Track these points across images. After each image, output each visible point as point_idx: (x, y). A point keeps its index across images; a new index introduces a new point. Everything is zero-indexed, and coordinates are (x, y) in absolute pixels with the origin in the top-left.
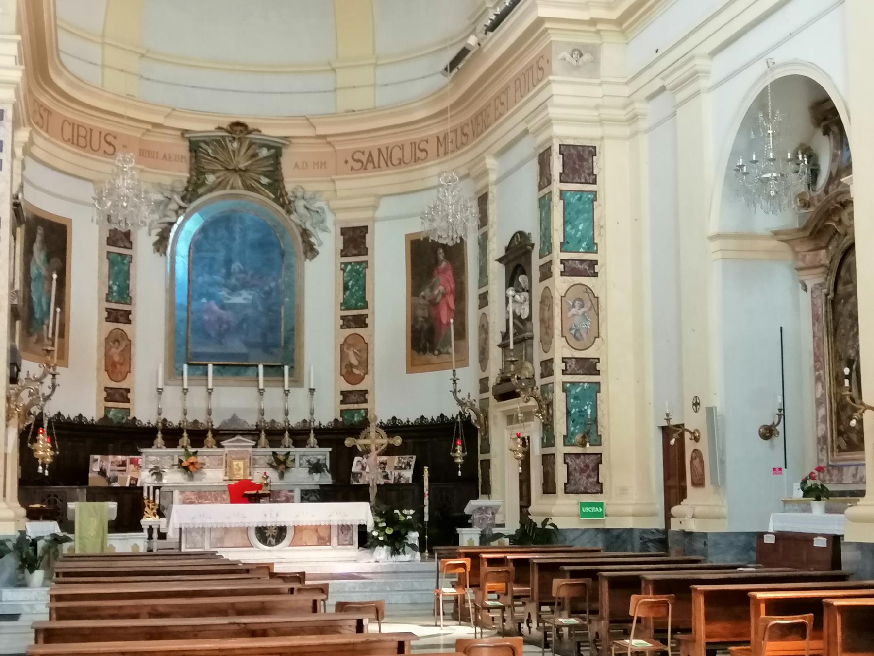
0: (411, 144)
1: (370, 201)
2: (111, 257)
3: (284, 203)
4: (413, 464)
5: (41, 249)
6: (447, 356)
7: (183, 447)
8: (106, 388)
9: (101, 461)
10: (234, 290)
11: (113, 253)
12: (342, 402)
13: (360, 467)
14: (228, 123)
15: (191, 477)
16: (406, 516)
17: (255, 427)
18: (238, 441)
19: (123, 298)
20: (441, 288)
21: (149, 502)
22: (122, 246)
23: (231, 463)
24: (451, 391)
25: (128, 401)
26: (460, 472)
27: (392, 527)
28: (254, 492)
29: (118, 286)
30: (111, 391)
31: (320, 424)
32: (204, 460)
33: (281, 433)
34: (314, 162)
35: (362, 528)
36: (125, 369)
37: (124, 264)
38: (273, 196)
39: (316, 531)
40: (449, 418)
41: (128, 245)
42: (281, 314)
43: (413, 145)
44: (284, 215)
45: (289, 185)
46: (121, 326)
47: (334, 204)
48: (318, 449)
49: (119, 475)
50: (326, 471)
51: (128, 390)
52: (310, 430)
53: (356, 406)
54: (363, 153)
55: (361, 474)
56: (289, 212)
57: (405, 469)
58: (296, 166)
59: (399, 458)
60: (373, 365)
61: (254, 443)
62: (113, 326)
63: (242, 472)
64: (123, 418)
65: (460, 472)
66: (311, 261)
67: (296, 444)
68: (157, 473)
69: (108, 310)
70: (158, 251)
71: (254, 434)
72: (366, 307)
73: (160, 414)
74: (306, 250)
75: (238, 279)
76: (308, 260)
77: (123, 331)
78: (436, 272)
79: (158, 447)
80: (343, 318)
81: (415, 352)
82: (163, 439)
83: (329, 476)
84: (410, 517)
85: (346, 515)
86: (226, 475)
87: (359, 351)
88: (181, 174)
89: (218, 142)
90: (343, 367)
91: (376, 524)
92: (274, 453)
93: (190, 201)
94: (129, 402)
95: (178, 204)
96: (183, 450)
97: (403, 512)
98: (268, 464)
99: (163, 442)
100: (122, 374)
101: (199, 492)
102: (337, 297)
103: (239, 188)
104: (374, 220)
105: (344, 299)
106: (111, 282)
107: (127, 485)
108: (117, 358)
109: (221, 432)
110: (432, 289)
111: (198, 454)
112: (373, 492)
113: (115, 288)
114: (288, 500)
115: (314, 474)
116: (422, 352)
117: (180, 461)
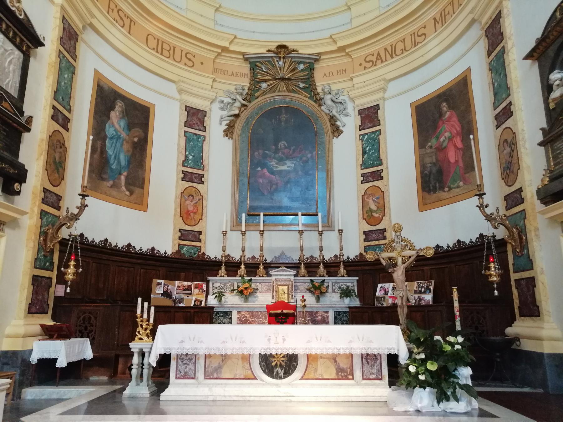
0: (411, 35)
1: (381, 84)
2: (188, 135)
4: (432, 288)
5: (122, 118)
7: (240, 276)
8: (180, 230)
9: (165, 285)
10: (281, 161)
11: (190, 132)
12: (365, 240)
13: (383, 292)
14: (275, 47)
15: (246, 300)
16: (452, 344)
17: (298, 261)
18: (283, 270)
20: (447, 134)
21: (142, 321)
22: (197, 128)
25: (200, 241)
26: (496, 292)
27: (436, 361)
28: (279, 312)
30: (185, 233)
31: (348, 258)
32: (257, 286)
33: (317, 266)
34: (337, 71)
35: (393, 359)
36: (197, 217)
37: (198, 141)
38: (309, 96)
39: (335, 360)
40: (114, 244)
41: (202, 129)
43: (413, 36)
44: (317, 107)
45: (320, 83)
47: (353, 94)
48: (346, 278)
49: (185, 297)
50: (354, 296)
51: (200, 233)
52: (340, 263)
53: (377, 243)
54: (373, 55)
55: (384, 298)
56: (320, 105)
57: (425, 292)
58: (325, 75)
59: (418, 283)
60: (389, 208)
61: (294, 272)
62: (187, 184)
64: (195, 254)
65: (496, 292)
67: (329, 274)
68: (219, 296)
70: (227, 135)
71: (295, 266)
72: (381, 164)
73: (224, 251)
75: (283, 153)
76: (335, 138)
78: (440, 123)
79: (221, 276)
80: (362, 175)
81: (426, 193)
82: (226, 269)
83: (358, 299)
84: (458, 347)
85: (371, 342)
86: (273, 299)
88: (246, 83)
89: (269, 61)
90: (365, 212)
91: (411, 352)
92: (312, 281)
94: (201, 242)
95: (241, 103)
96: (240, 278)
97: (448, 339)
98: (307, 290)
99: (226, 272)
100: (195, 221)
101: (253, 312)
102: (358, 160)
103: (284, 91)
104: (384, 99)
107: (192, 305)
108: (191, 208)
109: (272, 265)
110: (438, 138)
111: (252, 281)
112: (402, 314)
113: (191, 157)
114: (324, 321)
115: (345, 298)
116: (432, 192)
117: (238, 287)
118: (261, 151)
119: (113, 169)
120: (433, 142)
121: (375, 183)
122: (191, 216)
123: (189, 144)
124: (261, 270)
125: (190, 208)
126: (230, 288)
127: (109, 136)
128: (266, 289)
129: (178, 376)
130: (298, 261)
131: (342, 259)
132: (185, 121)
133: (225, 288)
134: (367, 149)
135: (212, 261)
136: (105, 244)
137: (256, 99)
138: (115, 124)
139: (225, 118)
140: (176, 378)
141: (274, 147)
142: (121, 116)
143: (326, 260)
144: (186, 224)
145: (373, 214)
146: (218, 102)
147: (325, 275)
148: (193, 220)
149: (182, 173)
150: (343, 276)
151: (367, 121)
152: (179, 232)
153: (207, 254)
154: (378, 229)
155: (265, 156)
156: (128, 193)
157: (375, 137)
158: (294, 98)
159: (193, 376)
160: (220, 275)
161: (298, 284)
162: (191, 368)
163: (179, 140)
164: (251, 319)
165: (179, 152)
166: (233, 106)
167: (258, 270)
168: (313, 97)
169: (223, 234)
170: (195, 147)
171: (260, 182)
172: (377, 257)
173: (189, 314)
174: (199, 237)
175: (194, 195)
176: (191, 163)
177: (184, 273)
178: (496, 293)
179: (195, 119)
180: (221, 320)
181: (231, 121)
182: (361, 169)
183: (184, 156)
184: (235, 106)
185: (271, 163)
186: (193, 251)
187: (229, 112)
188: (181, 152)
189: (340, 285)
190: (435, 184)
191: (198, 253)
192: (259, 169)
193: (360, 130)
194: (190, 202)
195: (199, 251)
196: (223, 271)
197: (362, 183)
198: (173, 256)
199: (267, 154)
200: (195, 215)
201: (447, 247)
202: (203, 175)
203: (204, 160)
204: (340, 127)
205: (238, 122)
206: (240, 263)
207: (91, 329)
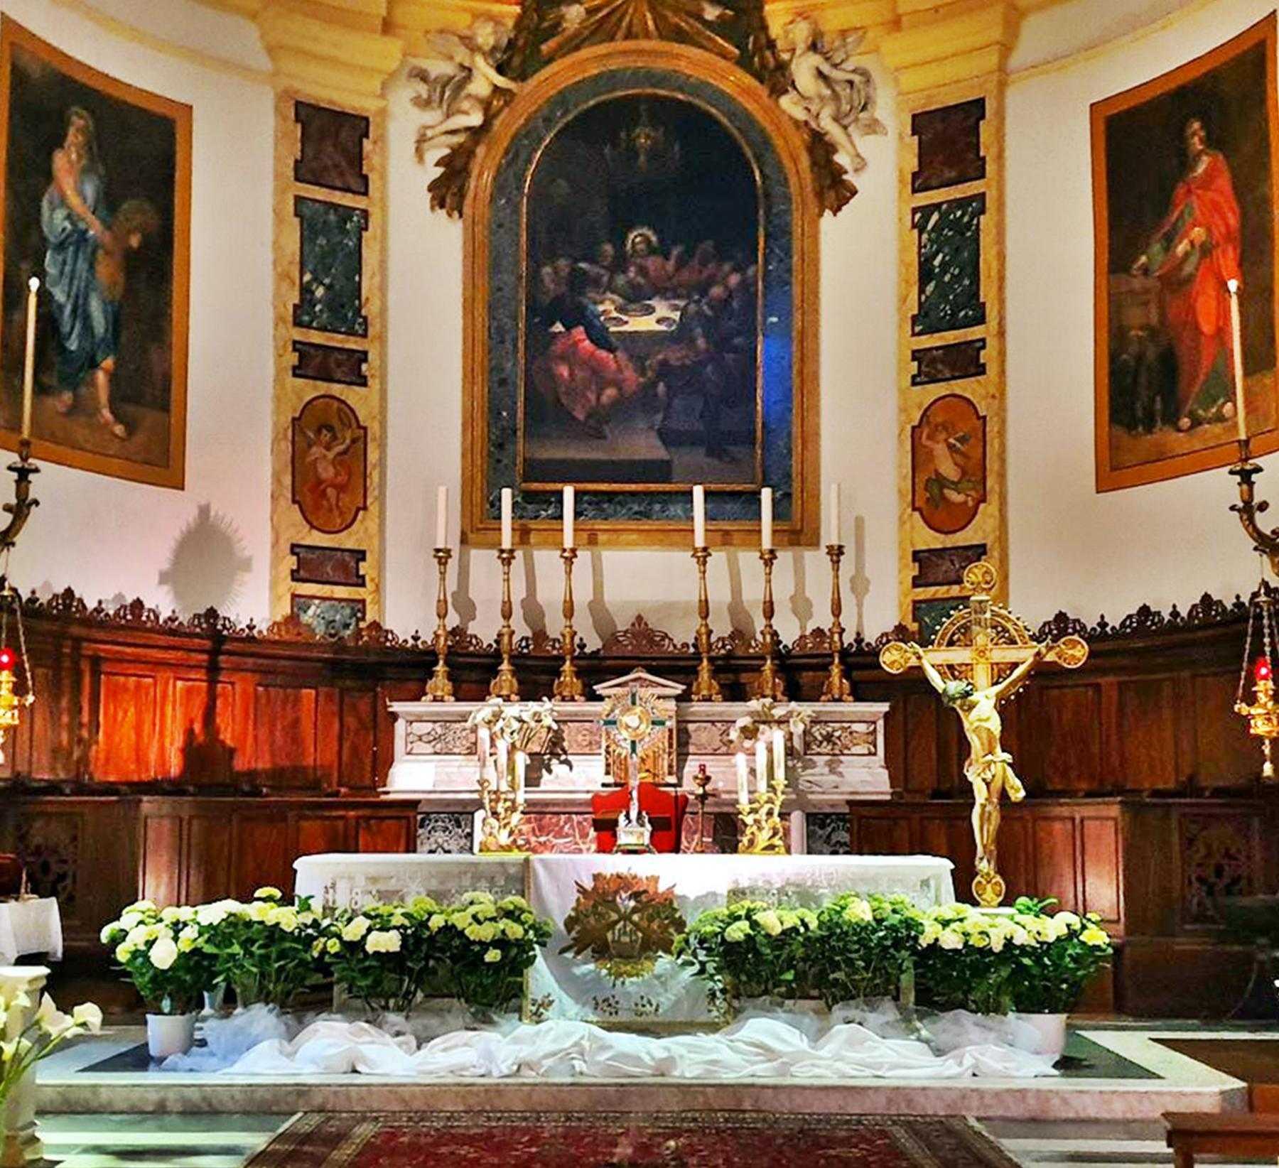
3: (764, 65)
6: (1218, 428)
8: (293, 546)
10: (636, 299)
12: (916, 583)
19: (344, 319)
20: (1198, 233)
22: (339, 184)
24: (1233, 508)
29: (329, 288)
30: (310, 556)
37: (346, 233)
40: (91, 605)
41: (354, 183)
46: (336, 389)
51: (360, 555)
52: (831, 656)
61: (679, 689)
62: (311, 389)
64: (347, 626)
67: (794, 693)
69: (298, 346)
72: (980, 320)
74: (822, 188)
75: (642, 271)
77: (343, 402)
78: (1181, 190)
80: (916, 355)
81: (1119, 431)
82: (450, 677)
86: (608, 773)
87: (962, 440)
90: (920, 487)
93: (522, 77)
94: (363, 585)
99: (449, 686)
100: (341, 513)
103: (647, 35)
105: (920, 304)
108: (326, 472)
110: (1169, 241)
113: (320, 292)
119: (72, 352)
120: (1152, 256)
121: (959, 386)
122: (328, 500)
125: (325, 469)
126: (466, 738)
127: (52, 239)
130: (692, 650)
131: (838, 644)
132: (296, 161)
133: (450, 738)
134: (936, 262)
135: (402, 649)
136: (68, 607)
138: (70, 193)
141: (608, 248)
142: (84, 162)
143: (785, 646)
144: (313, 527)
145: (946, 491)
148: (336, 513)
149: (295, 350)
150: (840, 700)
151: (941, 158)
152: (293, 553)
153: (387, 625)
154: (961, 544)
155: (579, 282)
156: (119, 429)
157: (966, 219)
160: (430, 697)
161: (691, 727)
163: (277, 235)
165: (282, 276)
166: (463, 94)
169: (436, 560)
171: (562, 375)
172: (913, 662)
173: (341, 824)
174: (358, 570)
175: (337, 425)
176: (321, 311)
177: (313, 692)
178: (1268, 769)
179: (330, 149)
180: (436, 842)
181: (456, 151)
182: (914, 334)
184: (469, 96)
185: (601, 308)
186: (338, 617)
187: (448, 116)
189: (830, 729)
190: (1153, 401)
191: (357, 625)
192: (558, 327)
193: (914, 191)
194: (324, 451)
195: (359, 615)
196: (440, 681)
197: (914, 384)
198: (277, 637)
199: (585, 272)
200: (342, 495)
201: (1171, 614)
202: (365, 353)
203: (367, 299)
204: (846, 172)
206: (497, 656)
207: (61, 871)
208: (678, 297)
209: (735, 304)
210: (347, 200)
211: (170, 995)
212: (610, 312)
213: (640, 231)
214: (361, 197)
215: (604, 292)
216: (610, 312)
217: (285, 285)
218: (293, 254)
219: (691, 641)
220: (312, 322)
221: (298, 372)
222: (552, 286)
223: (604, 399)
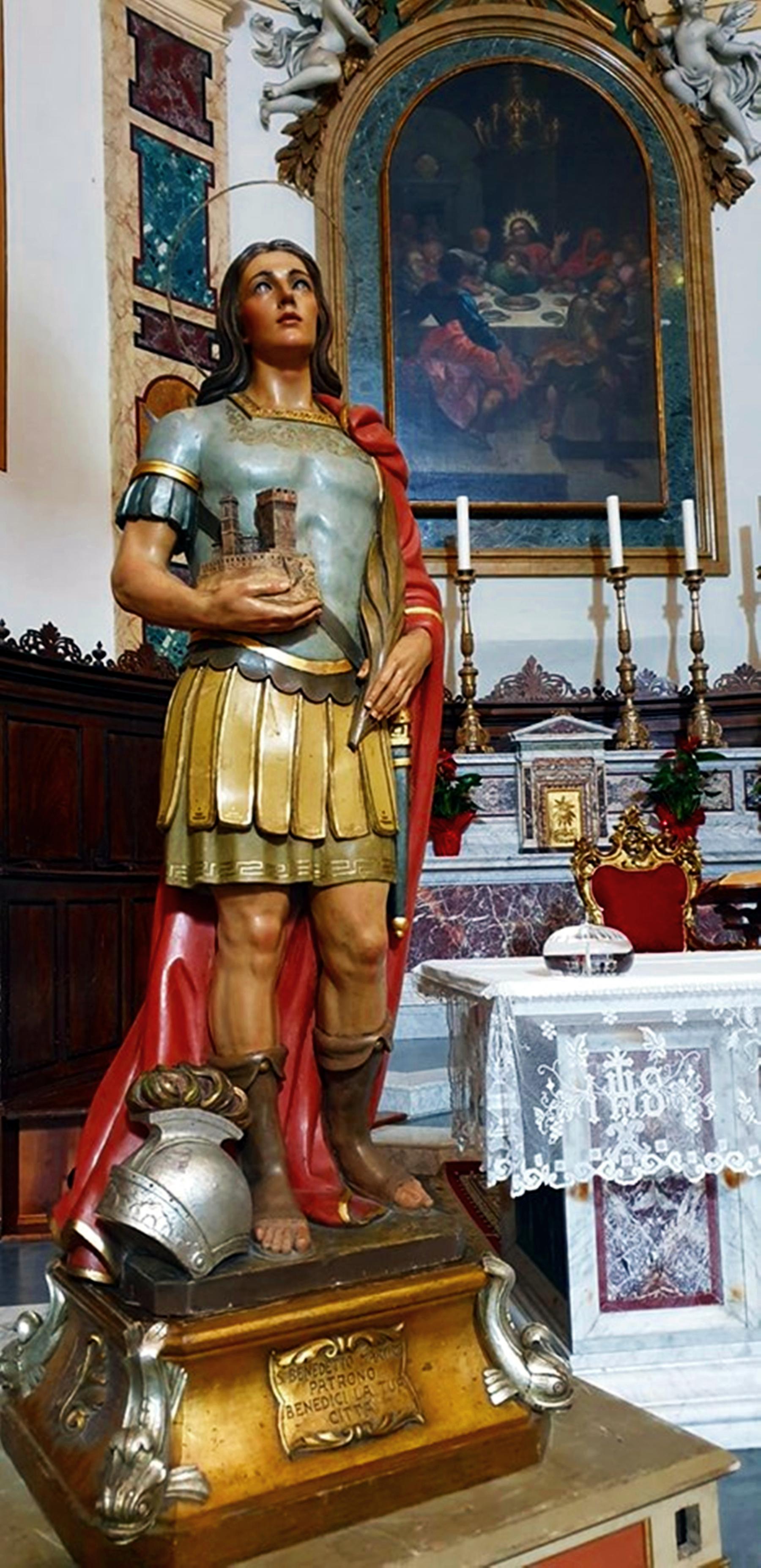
11: (154, 137)
18: (561, 728)
23: (543, 798)
41: (199, 130)
42: (301, 1147)
63: (576, 823)
66: (727, 207)
75: (524, 260)
106: (148, 228)
113: (163, 249)
118: (434, 249)
123: (153, 186)
124: (473, 728)
128: (493, 803)
129: (614, 1291)
130: (593, 696)
137: (401, 25)
139: (280, 97)
140: (605, 1306)
141: (484, 233)
146: (251, 25)
147: (717, 740)
158: (557, 32)
159: (707, 1287)
162: (685, 1239)
163: (111, 167)
164: (448, 916)
165: (117, 221)
166: (314, 47)
167: (459, 729)
168: (629, 33)
170: (177, 207)
176: (165, 272)
179: (170, 80)
183: (138, 240)
185: (478, 300)
188: (126, 221)
192: (431, 321)
198: (129, 670)
205: (333, 119)
208: (565, 290)
209: (629, 300)
210: (190, 145)
211: (200, 527)
212: (490, 305)
213: (519, 215)
214: (204, 146)
215: (481, 283)
216: (490, 305)
217: (123, 231)
218: (131, 196)
219: (591, 686)
220: (155, 284)
221: (140, 341)
222: (422, 275)
223: (487, 405)
